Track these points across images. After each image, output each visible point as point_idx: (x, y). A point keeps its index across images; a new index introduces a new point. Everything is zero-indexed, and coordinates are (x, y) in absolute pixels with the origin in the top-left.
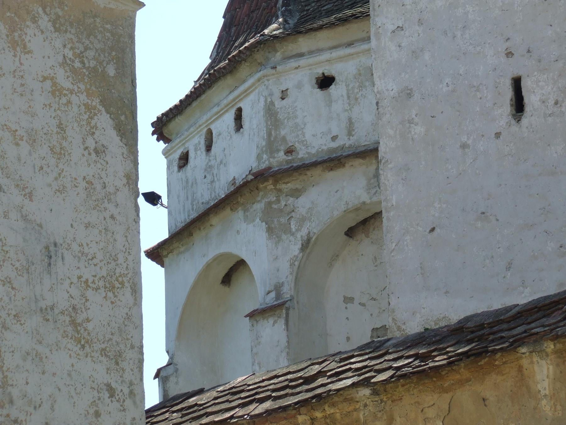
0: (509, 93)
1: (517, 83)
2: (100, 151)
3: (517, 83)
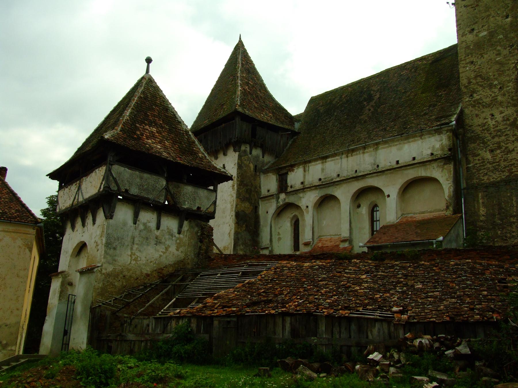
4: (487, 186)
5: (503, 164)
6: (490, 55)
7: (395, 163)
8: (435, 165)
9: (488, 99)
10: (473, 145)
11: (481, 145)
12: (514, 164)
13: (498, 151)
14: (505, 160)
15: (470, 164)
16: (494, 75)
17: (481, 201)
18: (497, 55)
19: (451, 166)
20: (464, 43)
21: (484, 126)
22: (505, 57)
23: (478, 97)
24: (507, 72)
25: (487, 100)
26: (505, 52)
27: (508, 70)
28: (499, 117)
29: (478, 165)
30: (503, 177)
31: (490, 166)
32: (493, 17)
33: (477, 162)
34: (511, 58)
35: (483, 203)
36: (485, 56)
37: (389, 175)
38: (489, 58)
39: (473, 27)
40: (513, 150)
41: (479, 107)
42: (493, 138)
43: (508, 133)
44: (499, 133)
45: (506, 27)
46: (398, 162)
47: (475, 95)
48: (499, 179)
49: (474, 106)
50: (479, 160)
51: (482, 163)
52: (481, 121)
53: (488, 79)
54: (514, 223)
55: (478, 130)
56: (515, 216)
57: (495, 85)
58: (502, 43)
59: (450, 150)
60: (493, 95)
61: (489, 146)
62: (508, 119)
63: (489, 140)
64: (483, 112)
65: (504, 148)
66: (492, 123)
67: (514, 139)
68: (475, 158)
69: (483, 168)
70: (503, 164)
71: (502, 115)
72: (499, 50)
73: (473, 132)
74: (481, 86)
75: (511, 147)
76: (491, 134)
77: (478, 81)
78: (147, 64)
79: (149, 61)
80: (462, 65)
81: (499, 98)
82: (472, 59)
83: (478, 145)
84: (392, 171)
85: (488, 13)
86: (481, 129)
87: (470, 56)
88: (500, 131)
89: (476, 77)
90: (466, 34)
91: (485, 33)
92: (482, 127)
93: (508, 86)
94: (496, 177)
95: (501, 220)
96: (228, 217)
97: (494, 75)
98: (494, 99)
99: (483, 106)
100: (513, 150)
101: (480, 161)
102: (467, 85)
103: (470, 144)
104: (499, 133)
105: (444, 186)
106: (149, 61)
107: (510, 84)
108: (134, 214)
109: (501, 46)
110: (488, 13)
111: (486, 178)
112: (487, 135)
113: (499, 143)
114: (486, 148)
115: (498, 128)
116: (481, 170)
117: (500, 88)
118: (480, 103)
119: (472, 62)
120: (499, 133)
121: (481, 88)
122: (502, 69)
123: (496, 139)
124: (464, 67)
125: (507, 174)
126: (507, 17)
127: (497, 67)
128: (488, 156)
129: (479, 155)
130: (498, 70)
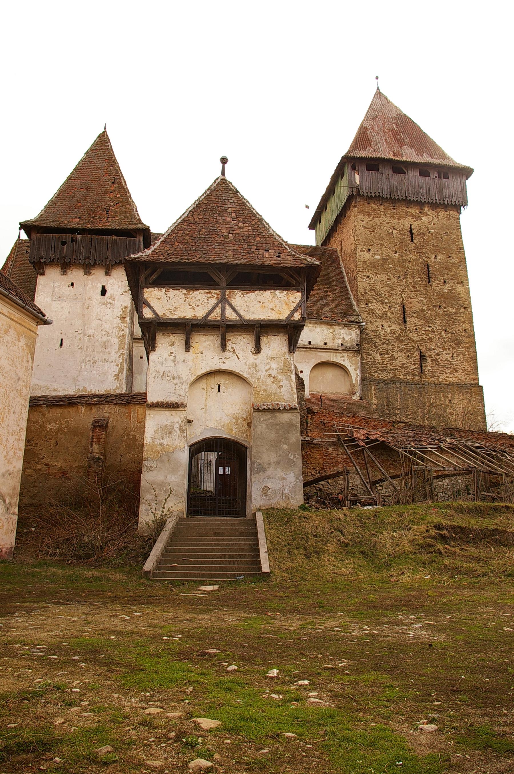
0: (60, 342)
1: (62, 340)
2: (28, 362)
3: (62, 340)
4: (379, 381)
5: (389, 367)
6: (382, 277)
7: (307, 343)
8: (345, 354)
9: (380, 312)
10: (367, 345)
11: (374, 347)
12: (397, 369)
13: (386, 356)
14: (391, 365)
15: (364, 360)
16: (385, 295)
17: (373, 392)
18: (388, 279)
19: (359, 358)
20: (362, 257)
21: (376, 332)
22: (394, 283)
23: (373, 308)
24: (395, 296)
25: (380, 313)
26: (395, 280)
27: (396, 295)
28: (388, 330)
29: (370, 363)
30: (389, 377)
31: (380, 366)
32: (385, 247)
33: (369, 360)
34: (398, 287)
35: (375, 394)
36: (379, 276)
37: (303, 353)
38: (382, 279)
39: (370, 248)
40: (397, 358)
41: (373, 316)
42: (383, 344)
43: (394, 344)
44: (387, 342)
45: (395, 260)
46: (310, 343)
47: (370, 305)
48: (386, 378)
49: (369, 314)
50: (371, 359)
51: (374, 362)
52: (374, 328)
53: (380, 295)
54: (398, 414)
55: (372, 334)
56: (398, 409)
57: (386, 303)
58: (392, 272)
59: (357, 345)
60: (384, 310)
61: (379, 349)
62: (394, 333)
63: (379, 345)
64: (376, 321)
65: (390, 355)
66: (382, 332)
67: (398, 350)
68: (368, 357)
69: (374, 366)
70: (389, 367)
71: (390, 328)
72: (389, 276)
73: (367, 334)
74: (375, 299)
75: (396, 356)
76: (381, 340)
77: (372, 294)
78: (221, 165)
79: (224, 161)
80: (360, 276)
81: (389, 314)
82: (368, 274)
83: (371, 346)
84: (308, 349)
85: (381, 242)
86: (374, 334)
87: (367, 271)
88: (388, 340)
89: (371, 290)
90: (364, 251)
91: (379, 257)
92: (375, 333)
93: (396, 308)
94: (383, 376)
95: (389, 410)
96: (114, 356)
97: (385, 295)
98: (385, 313)
99: (376, 316)
100: (397, 358)
101: (372, 360)
102: (363, 293)
103: (365, 344)
104: (387, 342)
105: (352, 375)
106: (224, 161)
107: (397, 306)
108: (256, 345)
109: (391, 273)
110: (381, 242)
111: (376, 374)
112: (378, 340)
113: (387, 350)
114: (377, 351)
115: (387, 338)
116: (372, 367)
117: (390, 307)
118: (374, 313)
119: (368, 277)
120: (387, 342)
121: (374, 301)
122: (391, 292)
123: (385, 346)
124: (361, 278)
125: (392, 376)
126: (396, 253)
127: (389, 289)
128: (379, 357)
129: (371, 355)
130: (388, 292)
